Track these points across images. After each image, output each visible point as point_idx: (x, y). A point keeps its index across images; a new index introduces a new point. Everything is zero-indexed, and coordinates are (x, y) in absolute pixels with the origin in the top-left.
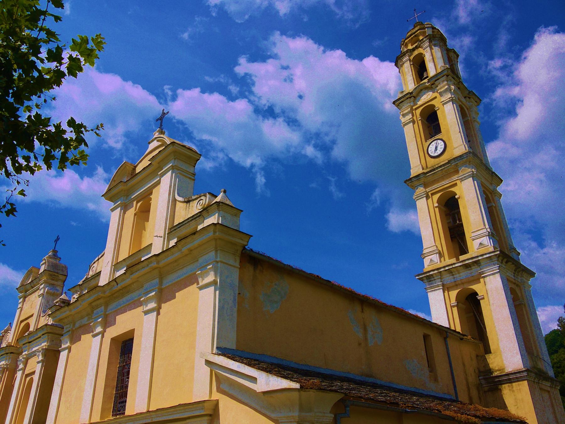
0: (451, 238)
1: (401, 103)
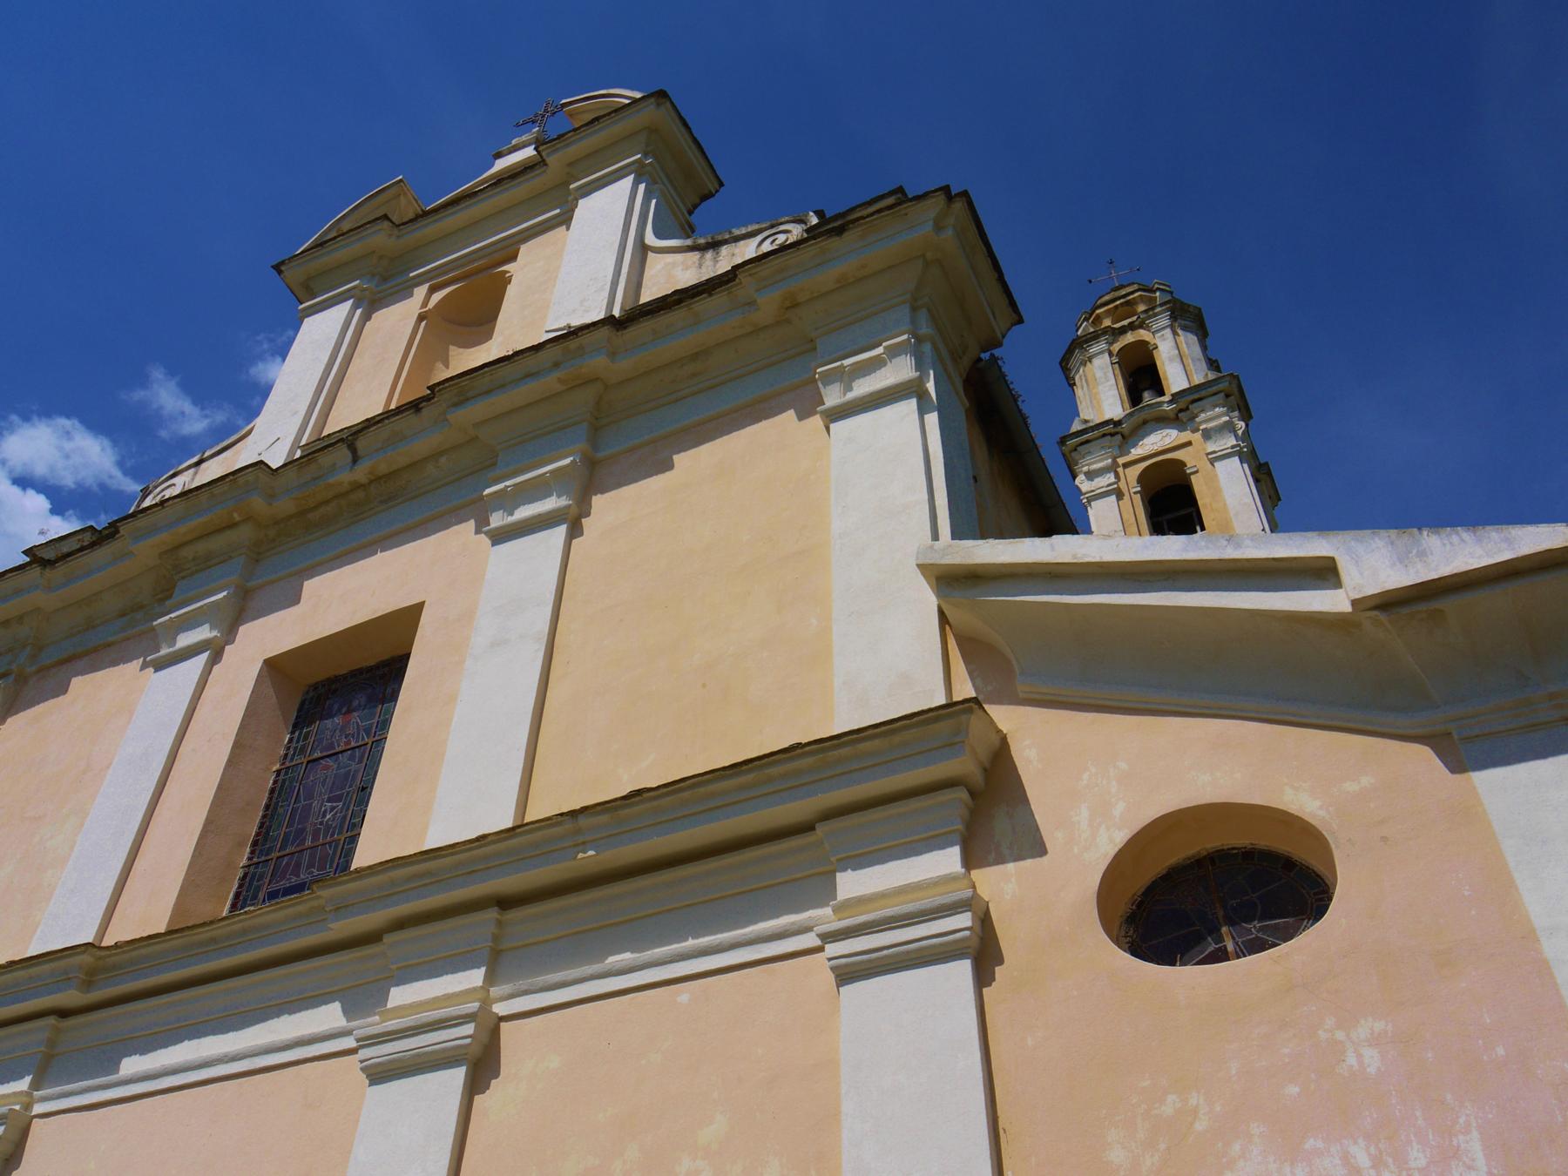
1: (1082, 444)
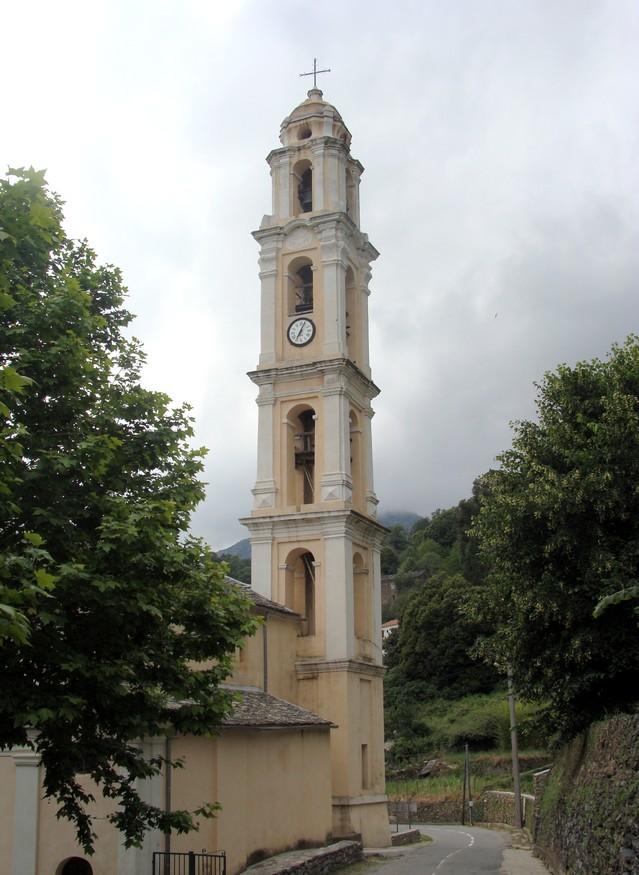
0: (296, 463)
